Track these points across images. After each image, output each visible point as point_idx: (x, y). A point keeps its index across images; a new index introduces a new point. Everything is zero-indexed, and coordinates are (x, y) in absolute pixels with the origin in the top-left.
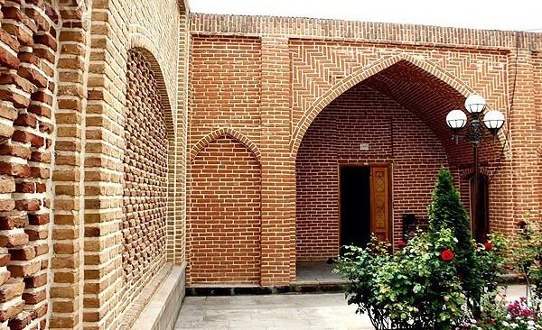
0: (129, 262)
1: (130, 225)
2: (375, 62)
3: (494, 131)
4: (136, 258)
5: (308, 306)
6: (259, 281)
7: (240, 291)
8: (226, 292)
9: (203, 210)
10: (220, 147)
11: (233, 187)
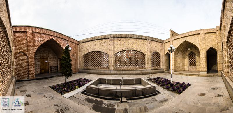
0: (5, 77)
1: (4, 69)
2: (46, 38)
3: (70, 51)
4: (6, 76)
5: (74, 101)
6: (29, 78)
7: (26, 80)
8: (23, 81)
9: (18, 66)
10: (20, 54)
11: (23, 62)
